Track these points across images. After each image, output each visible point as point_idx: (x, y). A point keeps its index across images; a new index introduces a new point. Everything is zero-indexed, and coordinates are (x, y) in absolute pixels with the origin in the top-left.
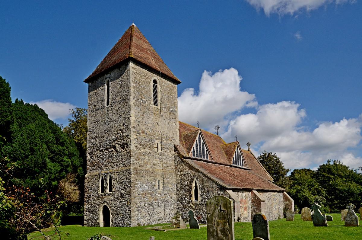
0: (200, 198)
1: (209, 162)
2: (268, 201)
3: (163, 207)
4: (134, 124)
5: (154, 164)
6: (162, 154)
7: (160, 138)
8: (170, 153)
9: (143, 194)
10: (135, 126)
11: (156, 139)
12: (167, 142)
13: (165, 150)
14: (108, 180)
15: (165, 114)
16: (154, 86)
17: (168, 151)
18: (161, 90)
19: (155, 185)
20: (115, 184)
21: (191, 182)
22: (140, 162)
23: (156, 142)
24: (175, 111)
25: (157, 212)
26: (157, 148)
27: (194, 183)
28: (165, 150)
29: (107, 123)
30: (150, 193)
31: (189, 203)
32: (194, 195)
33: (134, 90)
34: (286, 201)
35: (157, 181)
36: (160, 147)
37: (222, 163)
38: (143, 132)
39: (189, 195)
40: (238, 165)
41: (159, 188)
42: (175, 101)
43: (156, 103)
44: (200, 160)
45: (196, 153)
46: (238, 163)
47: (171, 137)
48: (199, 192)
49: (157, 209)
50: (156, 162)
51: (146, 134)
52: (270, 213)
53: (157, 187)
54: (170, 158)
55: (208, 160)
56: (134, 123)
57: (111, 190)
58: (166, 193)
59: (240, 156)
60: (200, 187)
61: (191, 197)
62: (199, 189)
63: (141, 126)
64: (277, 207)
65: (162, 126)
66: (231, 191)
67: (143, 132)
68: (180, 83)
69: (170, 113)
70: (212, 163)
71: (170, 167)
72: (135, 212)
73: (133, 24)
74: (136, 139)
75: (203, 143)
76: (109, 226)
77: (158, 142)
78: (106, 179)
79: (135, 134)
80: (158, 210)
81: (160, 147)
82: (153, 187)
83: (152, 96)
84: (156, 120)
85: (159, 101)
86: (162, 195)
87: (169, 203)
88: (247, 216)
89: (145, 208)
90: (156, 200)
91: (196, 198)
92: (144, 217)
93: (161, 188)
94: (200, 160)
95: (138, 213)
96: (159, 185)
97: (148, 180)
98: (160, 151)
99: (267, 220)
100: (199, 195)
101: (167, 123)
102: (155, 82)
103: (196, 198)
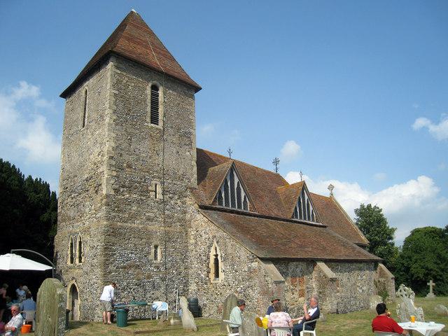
0: (222, 275)
1: (250, 215)
3: (162, 289)
5: (149, 219)
6: (163, 202)
9: (125, 268)
11: (153, 177)
15: (171, 137)
16: (152, 94)
17: (176, 197)
19: (149, 253)
20: (86, 250)
21: (209, 247)
23: (154, 182)
24: (190, 133)
25: (150, 297)
26: (156, 192)
27: (213, 252)
29: (81, 155)
31: (206, 284)
32: (213, 271)
36: (159, 190)
37: (273, 215)
38: (129, 166)
40: (313, 220)
41: (156, 258)
42: (191, 117)
43: (154, 119)
44: (232, 212)
45: (224, 200)
46: (305, 216)
50: (152, 215)
51: (135, 169)
52: (352, 299)
53: (151, 256)
55: (248, 211)
57: (80, 261)
58: (169, 265)
59: (308, 204)
60: (221, 256)
61: (209, 272)
62: (220, 260)
63: (126, 157)
64: (364, 288)
67: (129, 166)
69: (180, 136)
70: (255, 216)
73: (133, 10)
77: (157, 182)
79: (114, 169)
81: (159, 190)
82: (145, 256)
83: (149, 109)
86: (162, 269)
89: (129, 290)
91: (217, 275)
93: (159, 257)
94: (232, 212)
96: (156, 252)
99: (376, 306)
100: (220, 270)
101: (175, 151)
102: (155, 88)
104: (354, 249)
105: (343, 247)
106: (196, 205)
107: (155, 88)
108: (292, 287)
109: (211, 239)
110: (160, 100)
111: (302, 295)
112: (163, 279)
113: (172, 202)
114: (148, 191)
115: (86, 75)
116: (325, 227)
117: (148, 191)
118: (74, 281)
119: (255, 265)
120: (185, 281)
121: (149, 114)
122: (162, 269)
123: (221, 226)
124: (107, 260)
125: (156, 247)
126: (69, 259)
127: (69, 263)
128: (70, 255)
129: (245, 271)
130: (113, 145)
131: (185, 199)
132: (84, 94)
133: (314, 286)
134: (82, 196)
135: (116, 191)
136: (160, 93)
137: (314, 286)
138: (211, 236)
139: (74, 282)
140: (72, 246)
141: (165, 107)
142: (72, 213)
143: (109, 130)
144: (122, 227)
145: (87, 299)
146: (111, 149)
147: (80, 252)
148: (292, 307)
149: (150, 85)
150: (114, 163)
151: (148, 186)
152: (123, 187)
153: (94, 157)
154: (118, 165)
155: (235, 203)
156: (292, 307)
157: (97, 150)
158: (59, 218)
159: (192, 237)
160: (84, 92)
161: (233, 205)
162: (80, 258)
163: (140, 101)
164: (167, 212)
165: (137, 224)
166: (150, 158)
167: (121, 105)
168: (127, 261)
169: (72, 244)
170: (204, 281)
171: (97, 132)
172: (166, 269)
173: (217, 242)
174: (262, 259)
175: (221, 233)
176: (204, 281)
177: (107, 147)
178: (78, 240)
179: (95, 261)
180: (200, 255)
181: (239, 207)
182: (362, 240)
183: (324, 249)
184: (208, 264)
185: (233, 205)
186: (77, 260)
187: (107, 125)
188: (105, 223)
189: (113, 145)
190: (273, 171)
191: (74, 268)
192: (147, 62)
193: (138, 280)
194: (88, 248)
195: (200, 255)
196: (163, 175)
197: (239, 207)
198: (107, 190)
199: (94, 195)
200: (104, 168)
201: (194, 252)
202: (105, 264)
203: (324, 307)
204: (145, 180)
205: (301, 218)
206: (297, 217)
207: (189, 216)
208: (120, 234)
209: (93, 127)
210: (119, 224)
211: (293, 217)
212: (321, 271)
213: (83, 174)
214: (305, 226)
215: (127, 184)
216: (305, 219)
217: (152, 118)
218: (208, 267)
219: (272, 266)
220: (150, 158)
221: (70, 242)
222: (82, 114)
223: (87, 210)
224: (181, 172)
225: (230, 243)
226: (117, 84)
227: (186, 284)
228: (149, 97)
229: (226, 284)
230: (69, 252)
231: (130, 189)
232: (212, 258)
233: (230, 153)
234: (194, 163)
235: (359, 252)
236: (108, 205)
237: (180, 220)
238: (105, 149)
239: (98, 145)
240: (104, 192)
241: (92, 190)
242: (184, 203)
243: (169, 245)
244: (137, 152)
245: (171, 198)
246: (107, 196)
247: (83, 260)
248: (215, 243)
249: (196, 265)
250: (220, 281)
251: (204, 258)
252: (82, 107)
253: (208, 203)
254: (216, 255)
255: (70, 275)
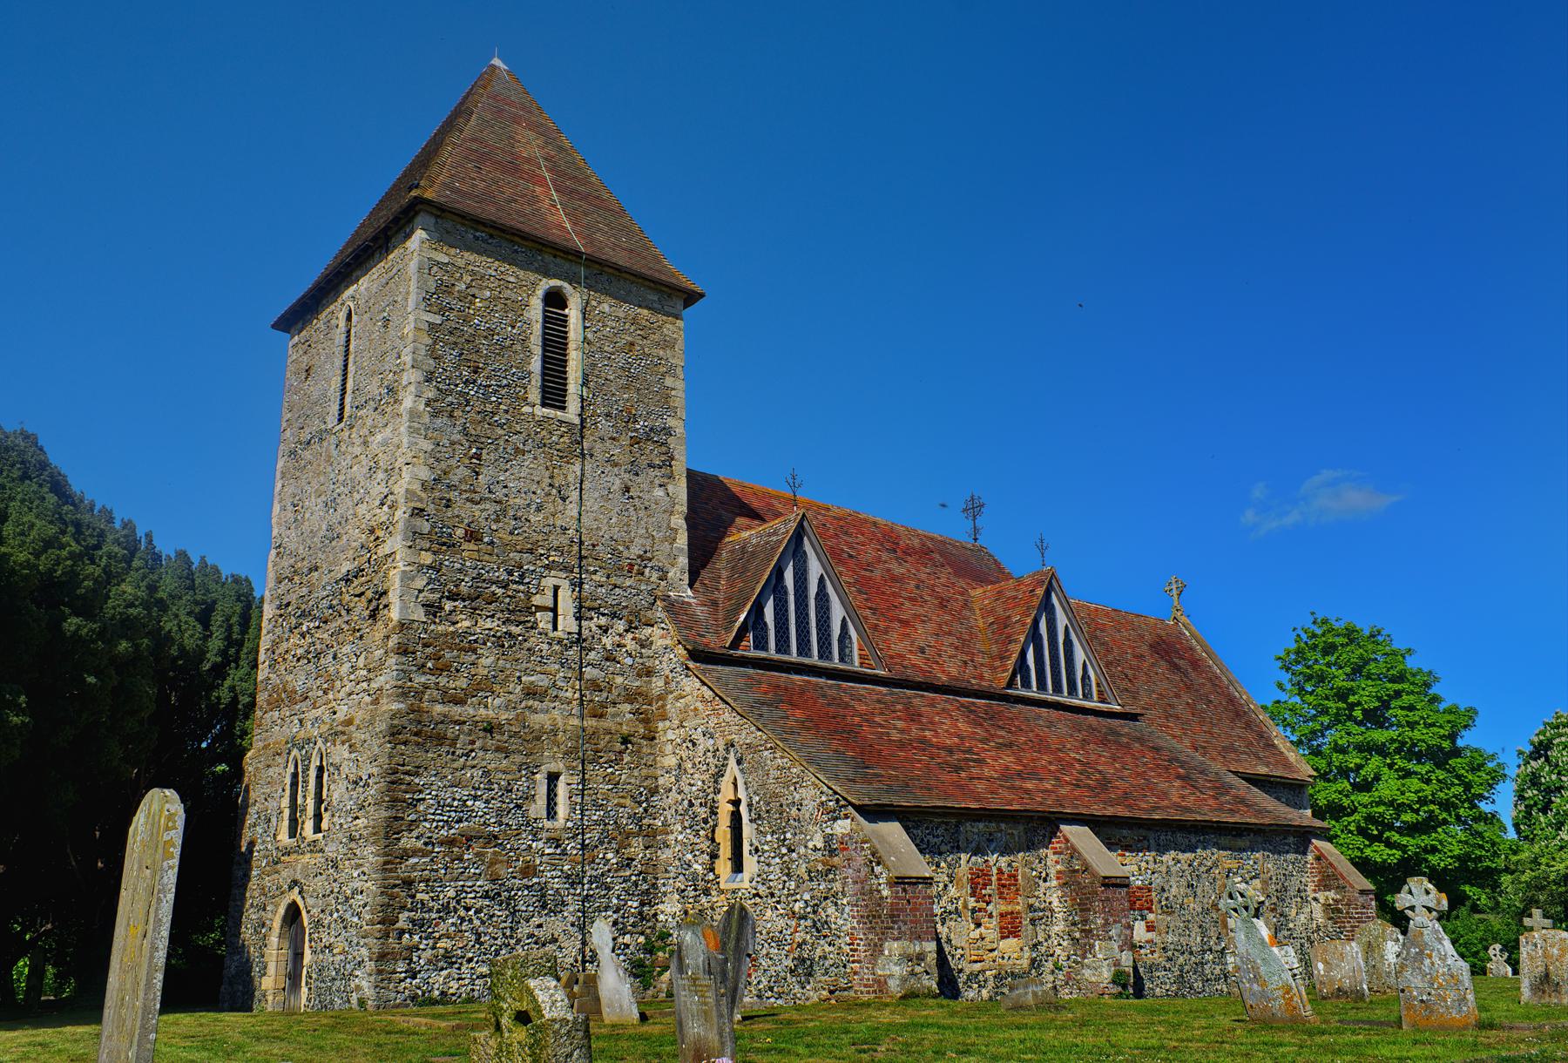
2: (1190, 886)
4: (421, 500)
5: (531, 693)
7: (575, 562)
8: (630, 636)
9: (451, 842)
10: (431, 509)
11: (547, 567)
12: (613, 580)
13: (603, 621)
14: (313, 773)
16: (546, 319)
17: (620, 626)
18: (590, 336)
20: (337, 792)
21: (719, 774)
22: (443, 681)
23: (549, 582)
25: (531, 936)
26: (554, 610)
28: (603, 621)
29: (330, 505)
30: (496, 837)
31: (707, 892)
32: (725, 851)
33: (435, 343)
34: (1327, 888)
35: (540, 778)
38: (473, 536)
39: (705, 845)
40: (1086, 696)
41: (551, 813)
43: (554, 394)
47: (640, 556)
48: (748, 830)
49: (536, 920)
51: (492, 543)
53: (538, 808)
54: (629, 661)
55: (856, 665)
56: (423, 495)
57: (317, 829)
60: (750, 805)
61: (714, 856)
65: (588, 504)
66: (897, 825)
67: (473, 536)
68: (702, 296)
69: (635, 441)
71: (627, 707)
72: (402, 932)
73: (496, 62)
74: (430, 567)
75: (821, 579)
76: (240, 996)
78: (306, 775)
80: (540, 926)
82: (519, 807)
83: (536, 365)
84: (552, 477)
85: (573, 387)
86: (571, 847)
87: (609, 889)
88: (1025, 963)
89: (462, 913)
90: (529, 871)
91: (738, 867)
92: (449, 958)
93: (562, 810)
95: (416, 938)
97: (486, 773)
98: (567, 623)
100: (746, 848)
101: (617, 485)
102: (555, 300)
103: (738, 867)
104: (1221, 788)
105: (1177, 783)
106: (681, 650)
107: (555, 300)
108: (972, 903)
109: (722, 753)
110: (572, 335)
111: (1010, 928)
112: (573, 880)
113: (608, 641)
114: (530, 610)
115: (348, 264)
116: (1134, 717)
117: (530, 610)
118: (296, 890)
119: (842, 827)
120: (645, 887)
121: (536, 380)
122: (571, 847)
123: (750, 712)
124: (396, 818)
125: (553, 778)
126: (286, 823)
127: (284, 837)
128: (287, 812)
129: (815, 849)
130: (425, 474)
131: (648, 630)
132: (342, 324)
133: (1056, 903)
134: (333, 626)
135: (432, 609)
136: (573, 313)
137: (1056, 903)
138: (721, 745)
139: (294, 895)
140: (294, 784)
141: (588, 355)
142: (298, 681)
143: (413, 431)
144: (445, 719)
145: (330, 947)
146: (417, 487)
147: (319, 800)
148: (978, 966)
149: (540, 293)
150: (426, 527)
151: (529, 595)
152: (453, 597)
153: (370, 512)
154: (436, 536)
155: (819, 630)
156: (978, 966)
157: (378, 490)
158: (261, 698)
159: (669, 748)
160: (342, 315)
161: (804, 648)
162: (318, 817)
163: (508, 342)
164: (590, 672)
165: (493, 708)
166: (538, 510)
167: (451, 356)
168: (460, 821)
169: (295, 775)
170: (701, 884)
171: (379, 437)
172: (584, 846)
173: (739, 762)
174: (864, 811)
175: (747, 734)
176: (701, 884)
177: (405, 482)
178: (315, 762)
179: (361, 822)
180: (691, 804)
181: (825, 652)
182: (1286, 764)
183: (1104, 784)
184: (713, 832)
185: (804, 648)
186: (309, 825)
187: (405, 418)
188: (395, 706)
189: (425, 474)
190: (967, 540)
191: (297, 850)
192: (540, 232)
193: (493, 881)
194: (343, 785)
195: (691, 804)
196: (579, 559)
197: (825, 652)
198: (404, 608)
199: (365, 627)
200: (395, 544)
201: (673, 794)
202: (391, 830)
203: (1087, 973)
204: (522, 576)
205: (1042, 686)
206: (1026, 684)
207: (661, 683)
208: (440, 739)
209: (369, 422)
210: (439, 708)
211: (1011, 684)
212: (1074, 853)
213: (336, 562)
214: (1054, 713)
215: (464, 589)
216: (1057, 689)
217: (544, 390)
218: (713, 840)
219: (893, 831)
220: (538, 510)
221: (291, 769)
222: (336, 381)
223: (345, 668)
224: (636, 550)
225: (775, 761)
226: (438, 296)
227: (649, 897)
228: (537, 328)
229: (762, 890)
230: (285, 802)
231: (475, 601)
232: (725, 809)
233: (793, 487)
234: (679, 522)
235: (1242, 801)
236: (405, 653)
237: (631, 696)
238: (400, 490)
239: (381, 475)
240: (395, 614)
241: (361, 608)
242: (644, 644)
243: (595, 773)
244: (500, 493)
245: (605, 630)
246: (403, 626)
247: (324, 825)
248: (732, 762)
249: (678, 835)
250: (747, 884)
251: (703, 812)
252: (339, 362)
253: (720, 641)
254: (736, 803)
255: (285, 875)
